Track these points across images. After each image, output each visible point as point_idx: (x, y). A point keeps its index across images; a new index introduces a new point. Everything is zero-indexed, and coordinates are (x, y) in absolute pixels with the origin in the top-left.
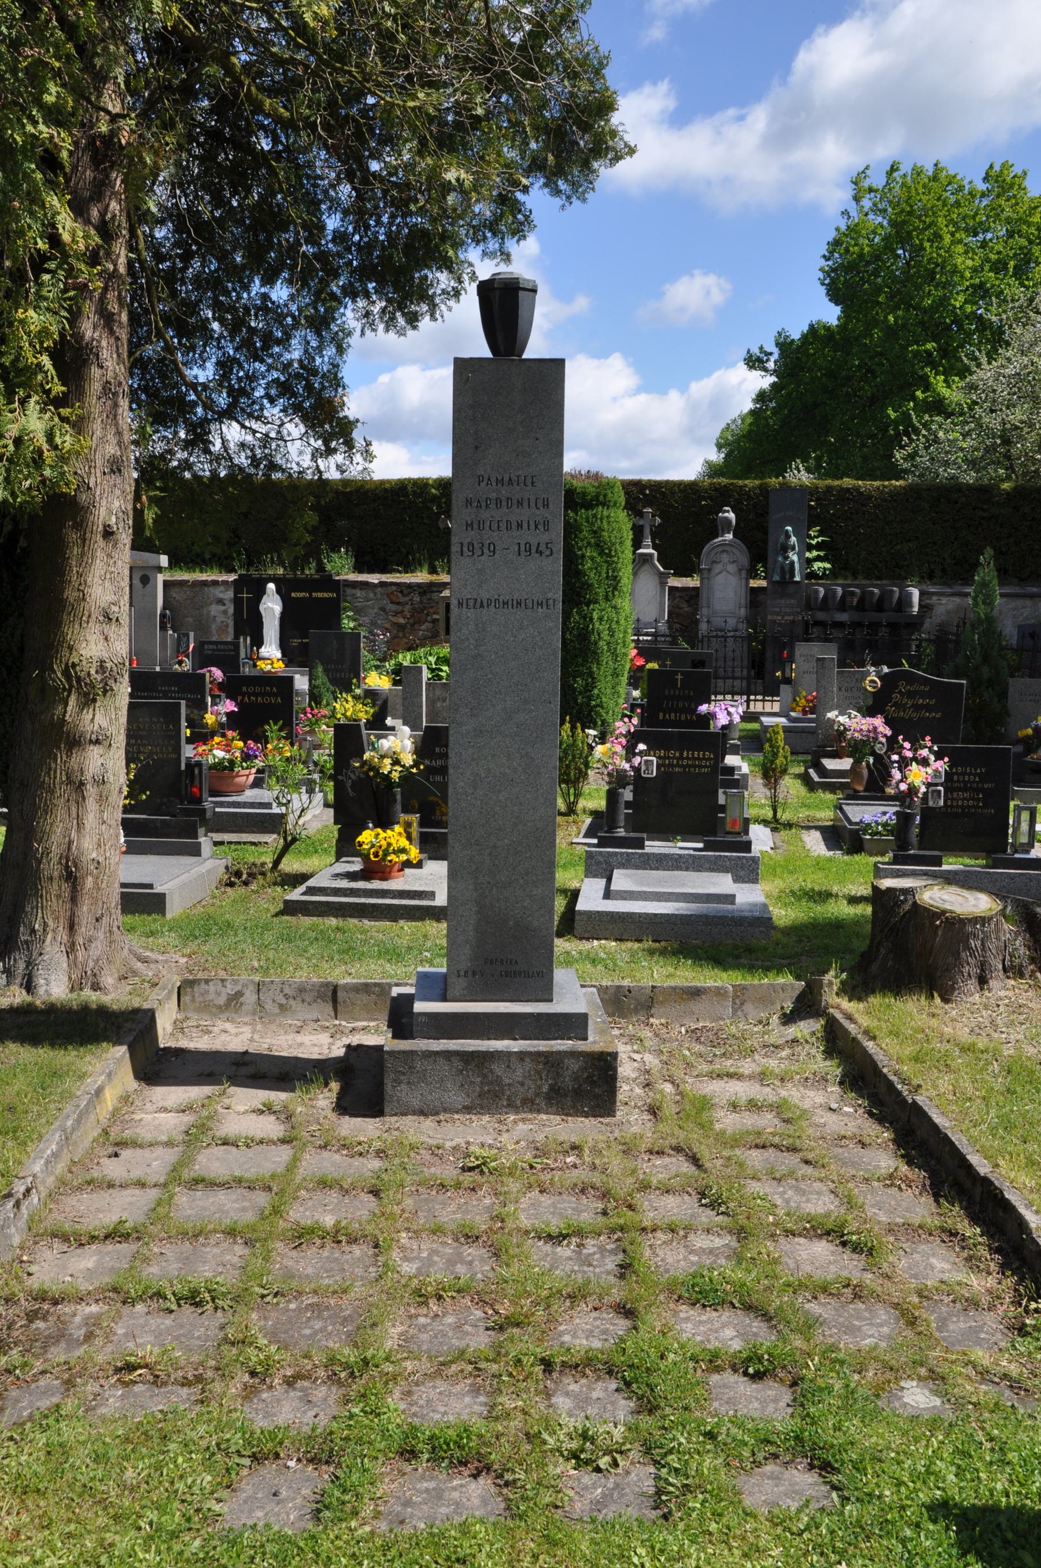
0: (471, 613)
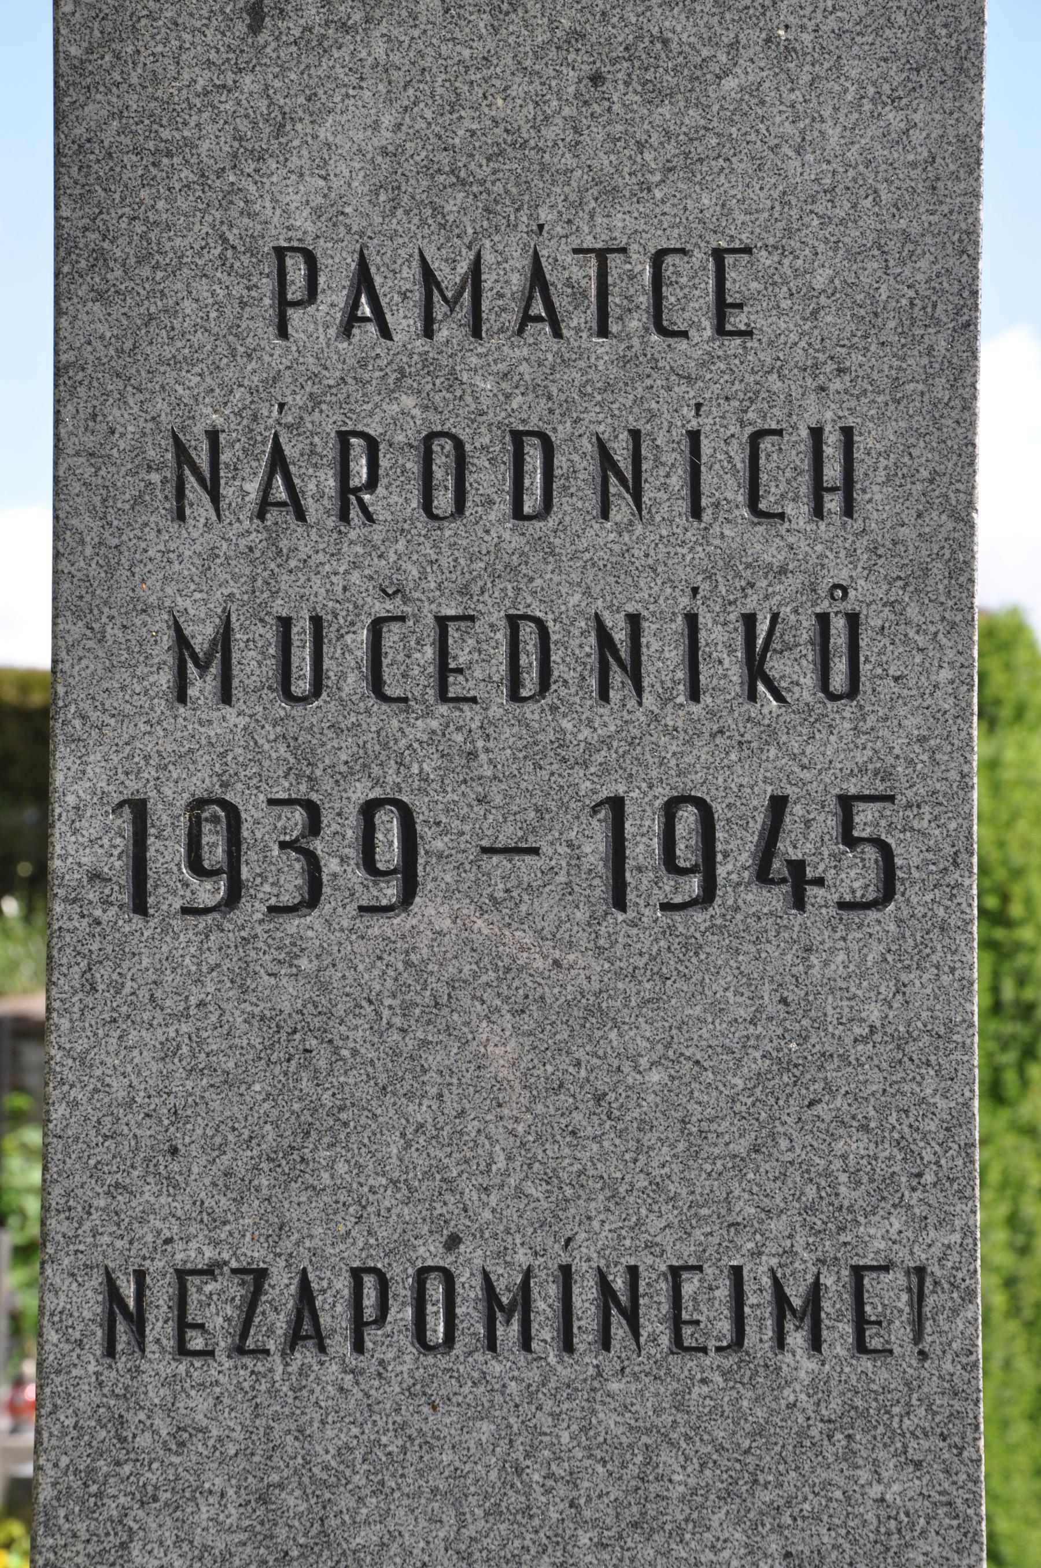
0: (212, 1396)
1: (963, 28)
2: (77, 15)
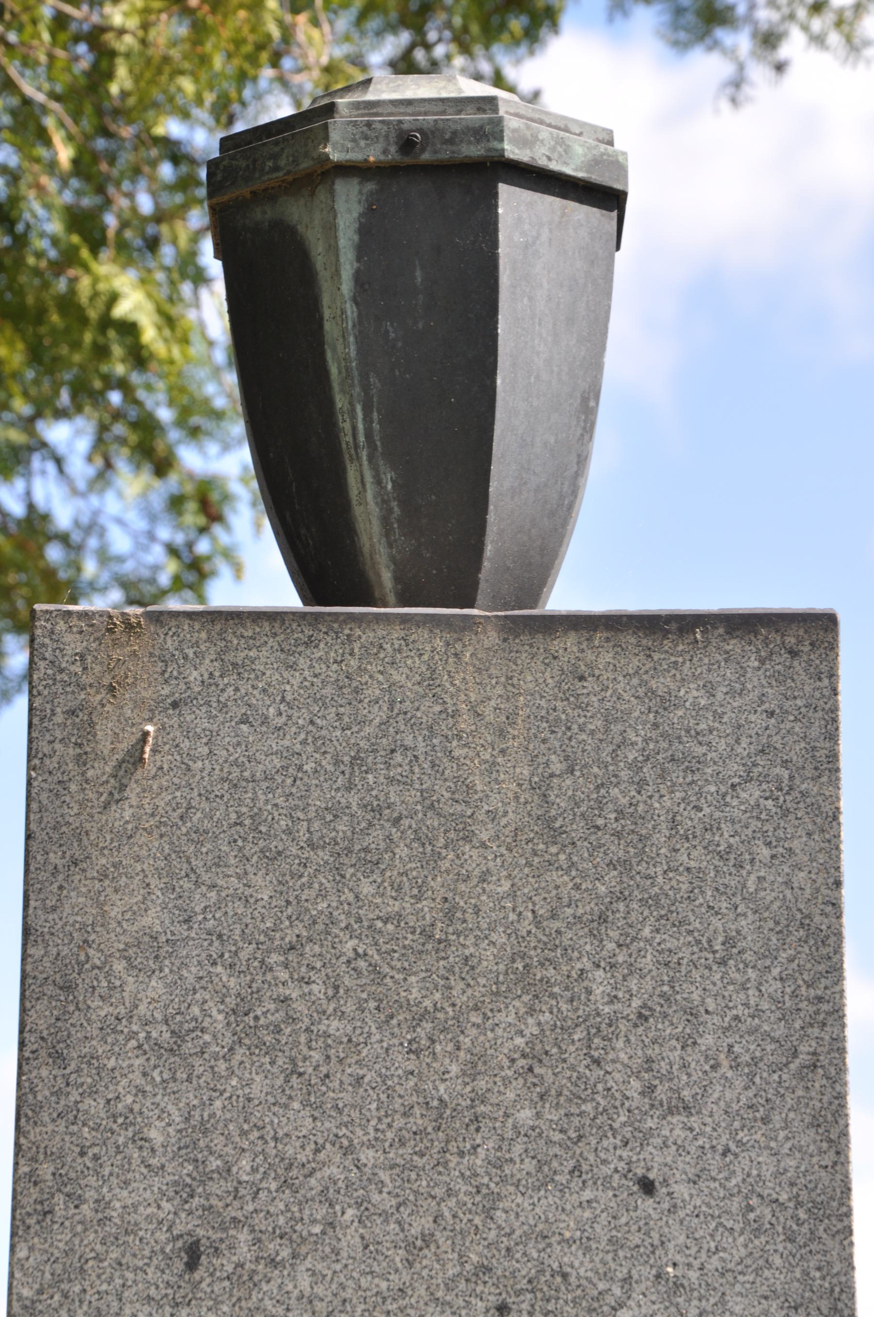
1: (835, 1271)
2: (31, 1260)
